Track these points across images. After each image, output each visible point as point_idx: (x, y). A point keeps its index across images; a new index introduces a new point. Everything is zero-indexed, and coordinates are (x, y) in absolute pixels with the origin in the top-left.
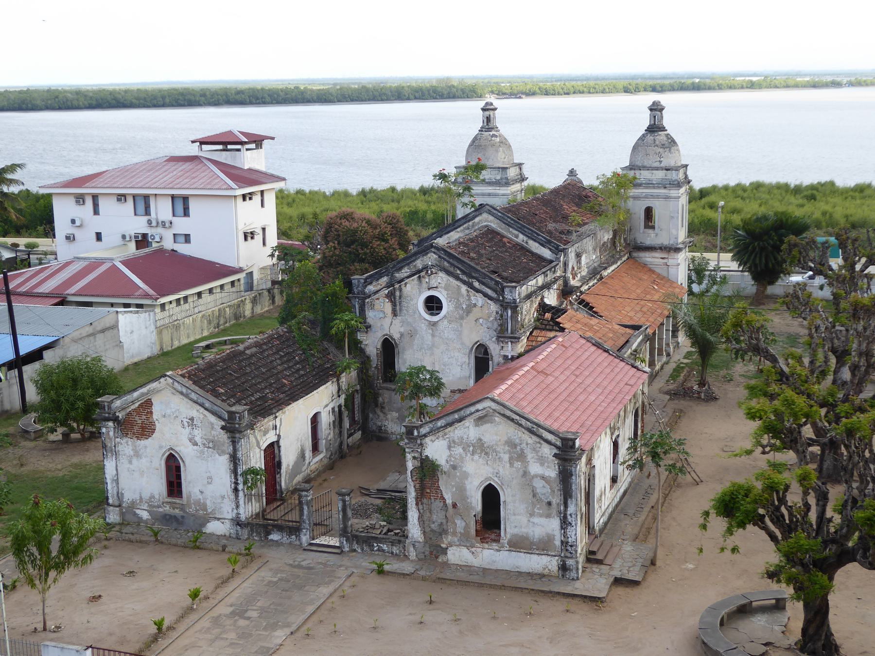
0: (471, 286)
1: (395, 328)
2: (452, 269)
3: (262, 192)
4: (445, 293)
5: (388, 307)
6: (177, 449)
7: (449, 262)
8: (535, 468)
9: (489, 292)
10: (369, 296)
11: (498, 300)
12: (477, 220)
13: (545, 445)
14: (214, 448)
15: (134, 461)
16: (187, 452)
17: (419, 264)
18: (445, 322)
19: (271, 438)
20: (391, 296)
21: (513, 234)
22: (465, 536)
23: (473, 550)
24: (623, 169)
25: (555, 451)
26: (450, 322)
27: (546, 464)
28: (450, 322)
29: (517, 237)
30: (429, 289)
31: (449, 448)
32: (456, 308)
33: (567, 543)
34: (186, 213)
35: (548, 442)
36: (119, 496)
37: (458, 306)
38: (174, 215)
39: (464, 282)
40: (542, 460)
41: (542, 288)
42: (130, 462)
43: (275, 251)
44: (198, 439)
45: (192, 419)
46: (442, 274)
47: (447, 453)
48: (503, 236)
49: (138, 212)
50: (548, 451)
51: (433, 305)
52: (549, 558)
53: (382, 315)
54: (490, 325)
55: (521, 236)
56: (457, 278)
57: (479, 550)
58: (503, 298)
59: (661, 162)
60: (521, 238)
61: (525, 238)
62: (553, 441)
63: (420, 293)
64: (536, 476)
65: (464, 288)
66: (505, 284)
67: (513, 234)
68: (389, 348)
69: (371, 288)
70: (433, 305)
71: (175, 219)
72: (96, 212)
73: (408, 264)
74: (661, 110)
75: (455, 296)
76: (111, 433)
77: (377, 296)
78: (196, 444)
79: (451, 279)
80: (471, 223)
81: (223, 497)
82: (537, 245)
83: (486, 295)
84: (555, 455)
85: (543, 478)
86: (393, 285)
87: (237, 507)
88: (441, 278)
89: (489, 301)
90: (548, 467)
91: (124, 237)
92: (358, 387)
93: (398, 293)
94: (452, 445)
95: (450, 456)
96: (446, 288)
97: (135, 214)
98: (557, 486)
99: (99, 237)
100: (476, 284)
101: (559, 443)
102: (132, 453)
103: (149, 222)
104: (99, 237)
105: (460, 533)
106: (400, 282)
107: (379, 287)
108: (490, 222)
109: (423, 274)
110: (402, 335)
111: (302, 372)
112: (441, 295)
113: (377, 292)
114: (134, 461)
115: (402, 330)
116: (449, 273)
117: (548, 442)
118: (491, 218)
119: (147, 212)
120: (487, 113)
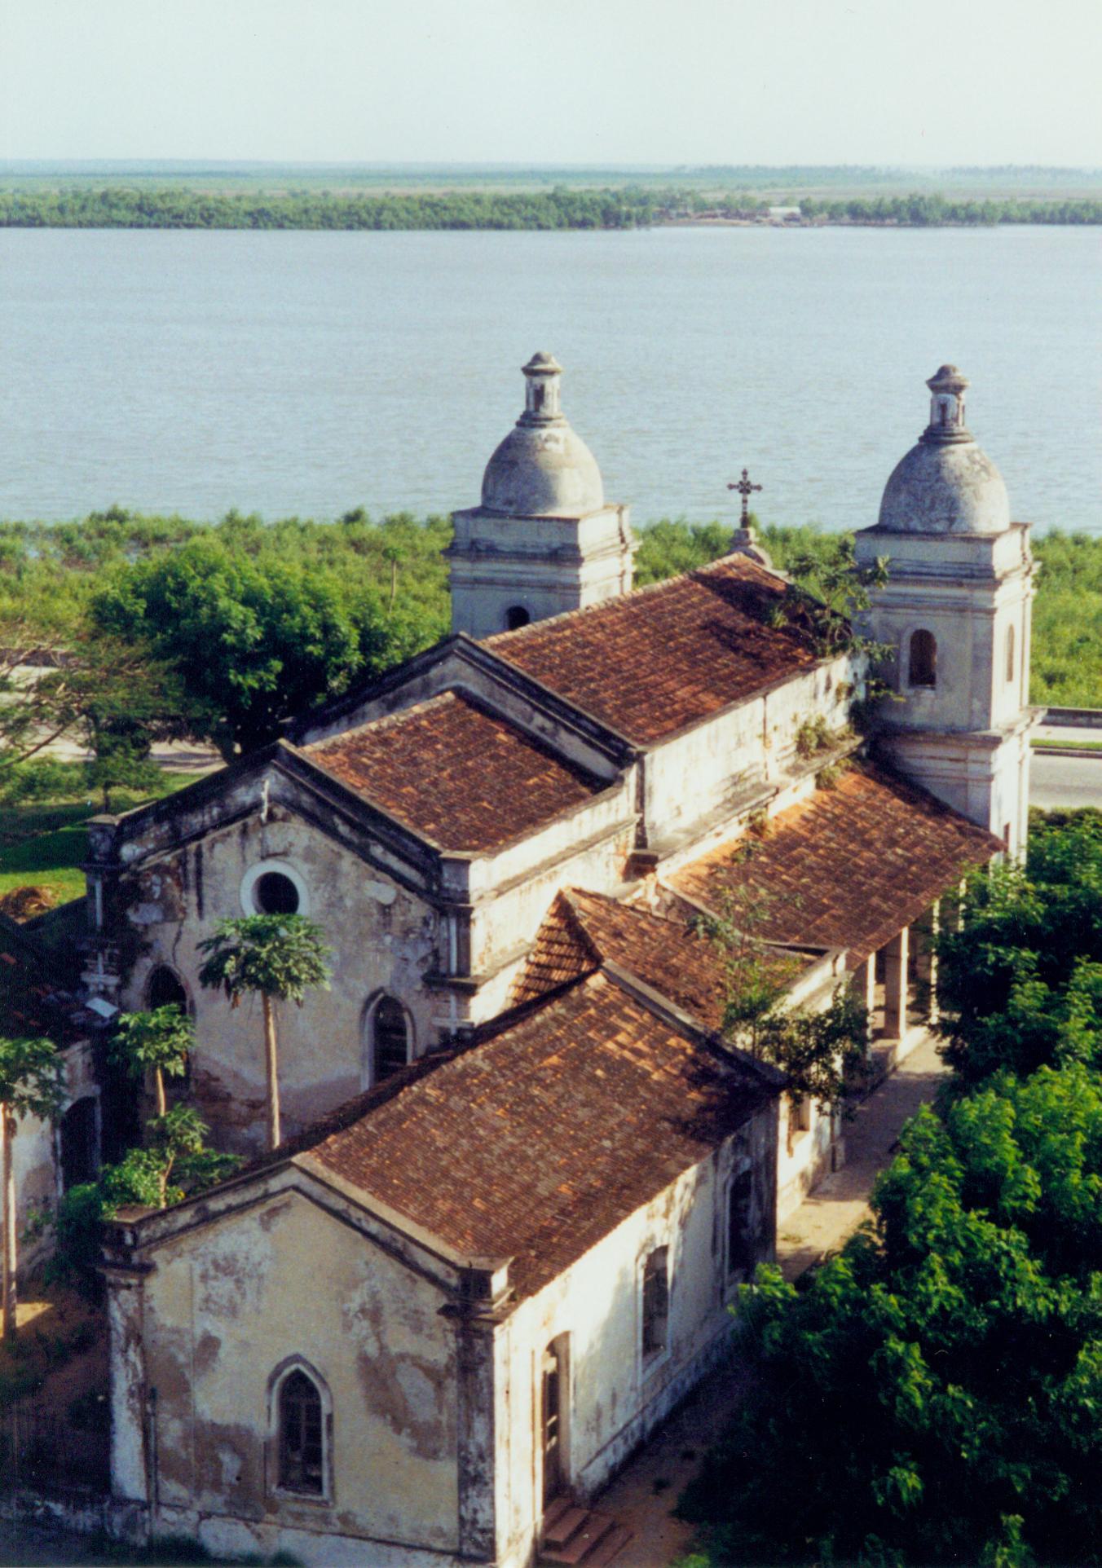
2: (318, 811)
4: (305, 867)
7: (312, 794)
11: (429, 891)
13: (423, 1283)
23: (259, 1527)
24: (860, 534)
27: (426, 1331)
29: (530, 720)
30: (263, 858)
33: (474, 1522)
35: (432, 1279)
43: (236, 634)
46: (297, 824)
50: (429, 1299)
55: (539, 720)
56: (332, 833)
57: (273, 1529)
58: (440, 887)
61: (548, 725)
62: (442, 1275)
64: (402, 1357)
66: (446, 854)
74: (958, 389)
82: (576, 741)
83: (399, 879)
84: (446, 1311)
85: (416, 1361)
88: (299, 834)
89: (407, 894)
90: (430, 1337)
93: (191, 866)
94: (212, 1272)
96: (309, 855)
100: (377, 851)
101: (454, 1281)
105: (230, 1485)
108: (467, 680)
116: (312, 819)
117: (432, 1279)
120: (537, 380)
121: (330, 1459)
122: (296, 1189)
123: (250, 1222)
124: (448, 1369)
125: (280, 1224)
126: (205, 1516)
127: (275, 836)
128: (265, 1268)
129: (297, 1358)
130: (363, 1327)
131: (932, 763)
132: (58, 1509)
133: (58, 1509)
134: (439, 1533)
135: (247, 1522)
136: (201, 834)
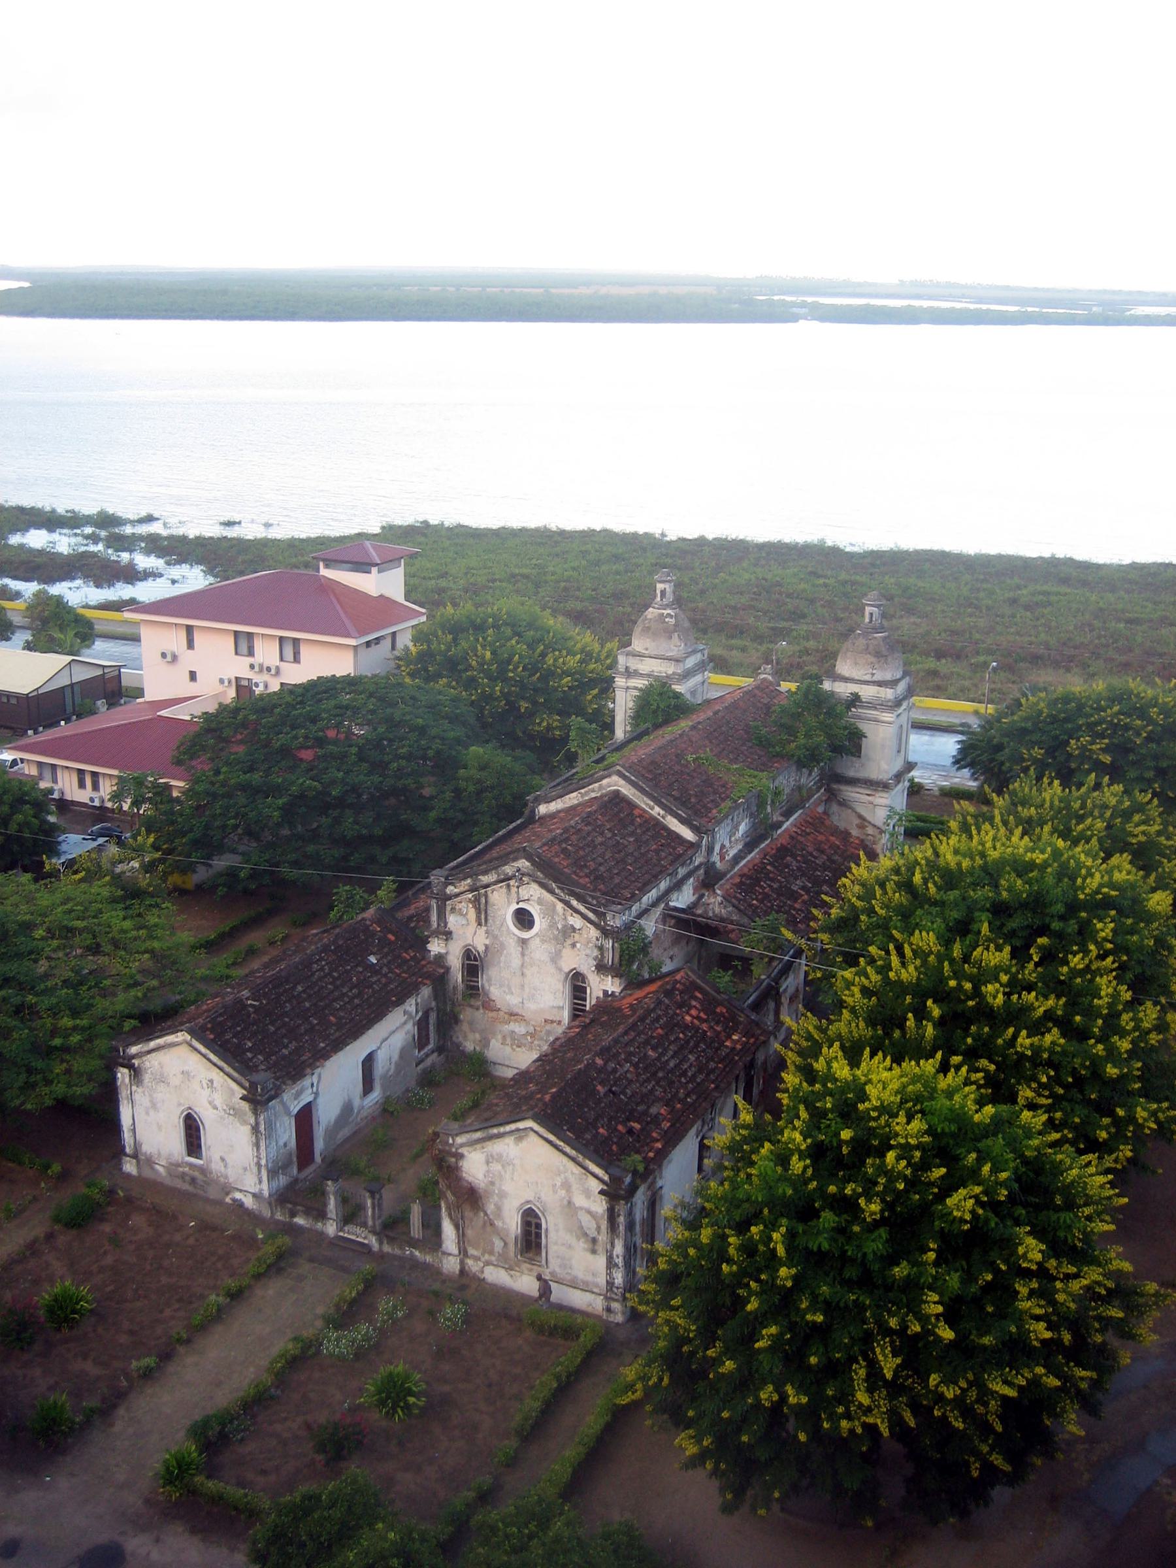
0: (567, 904)
1: (479, 941)
3: (394, 634)
5: (472, 914)
6: (197, 1109)
8: (580, 1201)
9: (591, 915)
10: (450, 898)
12: (605, 782)
13: (591, 1178)
14: (234, 1115)
15: (152, 1112)
16: (209, 1118)
17: (508, 869)
18: (537, 940)
19: (307, 1098)
20: (476, 902)
21: (647, 804)
22: (503, 1256)
25: (601, 1186)
26: (543, 941)
28: (543, 941)
29: (652, 809)
31: (488, 1163)
32: (550, 926)
33: (613, 1283)
34: (296, 659)
36: (137, 1146)
37: (552, 925)
38: (282, 659)
39: (561, 900)
40: (587, 1193)
41: (668, 891)
42: (147, 1113)
44: (218, 1103)
45: (211, 1081)
46: (534, 886)
47: (485, 1168)
48: (636, 806)
49: (239, 650)
51: (524, 919)
52: (593, 1296)
53: (464, 922)
54: (588, 952)
55: (657, 809)
56: (551, 892)
59: (873, 674)
60: (657, 811)
61: (662, 812)
63: (509, 903)
64: (581, 1208)
65: (560, 906)
67: (647, 804)
68: (473, 964)
69: (450, 889)
70: (524, 919)
71: (283, 665)
72: (190, 645)
73: (496, 868)
75: (549, 912)
76: (127, 1080)
77: (459, 899)
78: (216, 1108)
79: (543, 891)
80: (597, 785)
81: (245, 1169)
82: (675, 821)
84: (602, 1192)
85: (589, 1212)
86: (476, 889)
87: (260, 1182)
88: (532, 891)
91: (222, 681)
92: (433, 1004)
93: (483, 900)
95: (488, 1171)
96: (540, 902)
97: (236, 653)
98: (604, 1224)
99: (193, 676)
102: (149, 1104)
103: (252, 667)
104: (193, 676)
106: (487, 886)
107: (462, 889)
109: (512, 882)
110: (487, 947)
111: (356, 1001)
112: (534, 910)
113: (457, 895)
114: (152, 1112)
115: (487, 942)
116: (543, 885)
118: (622, 782)
119: (251, 653)
121: (546, 1247)
122: (532, 1129)
123: (509, 1140)
124: (603, 1216)
125: (524, 1144)
126: (488, 1263)
127: (524, 892)
128: (515, 1162)
129: (528, 1202)
130: (563, 1193)
131: (853, 795)
132: (417, 1253)
133: (417, 1253)
134: (597, 1286)
135: (506, 1269)
136: (487, 886)
